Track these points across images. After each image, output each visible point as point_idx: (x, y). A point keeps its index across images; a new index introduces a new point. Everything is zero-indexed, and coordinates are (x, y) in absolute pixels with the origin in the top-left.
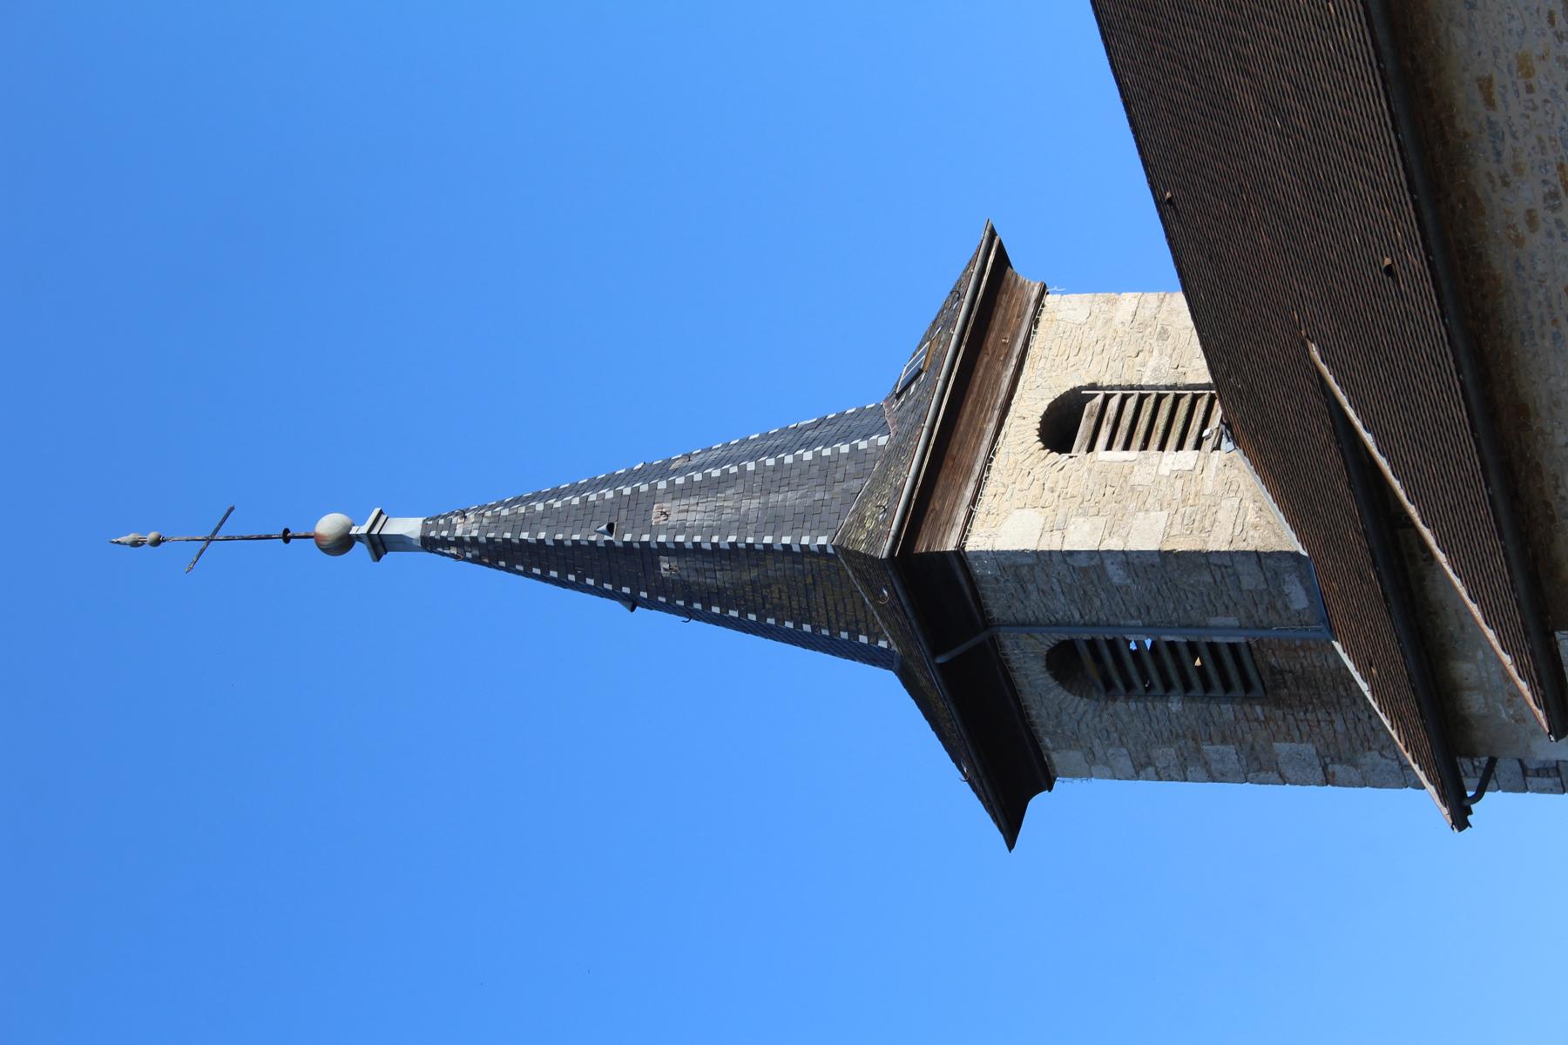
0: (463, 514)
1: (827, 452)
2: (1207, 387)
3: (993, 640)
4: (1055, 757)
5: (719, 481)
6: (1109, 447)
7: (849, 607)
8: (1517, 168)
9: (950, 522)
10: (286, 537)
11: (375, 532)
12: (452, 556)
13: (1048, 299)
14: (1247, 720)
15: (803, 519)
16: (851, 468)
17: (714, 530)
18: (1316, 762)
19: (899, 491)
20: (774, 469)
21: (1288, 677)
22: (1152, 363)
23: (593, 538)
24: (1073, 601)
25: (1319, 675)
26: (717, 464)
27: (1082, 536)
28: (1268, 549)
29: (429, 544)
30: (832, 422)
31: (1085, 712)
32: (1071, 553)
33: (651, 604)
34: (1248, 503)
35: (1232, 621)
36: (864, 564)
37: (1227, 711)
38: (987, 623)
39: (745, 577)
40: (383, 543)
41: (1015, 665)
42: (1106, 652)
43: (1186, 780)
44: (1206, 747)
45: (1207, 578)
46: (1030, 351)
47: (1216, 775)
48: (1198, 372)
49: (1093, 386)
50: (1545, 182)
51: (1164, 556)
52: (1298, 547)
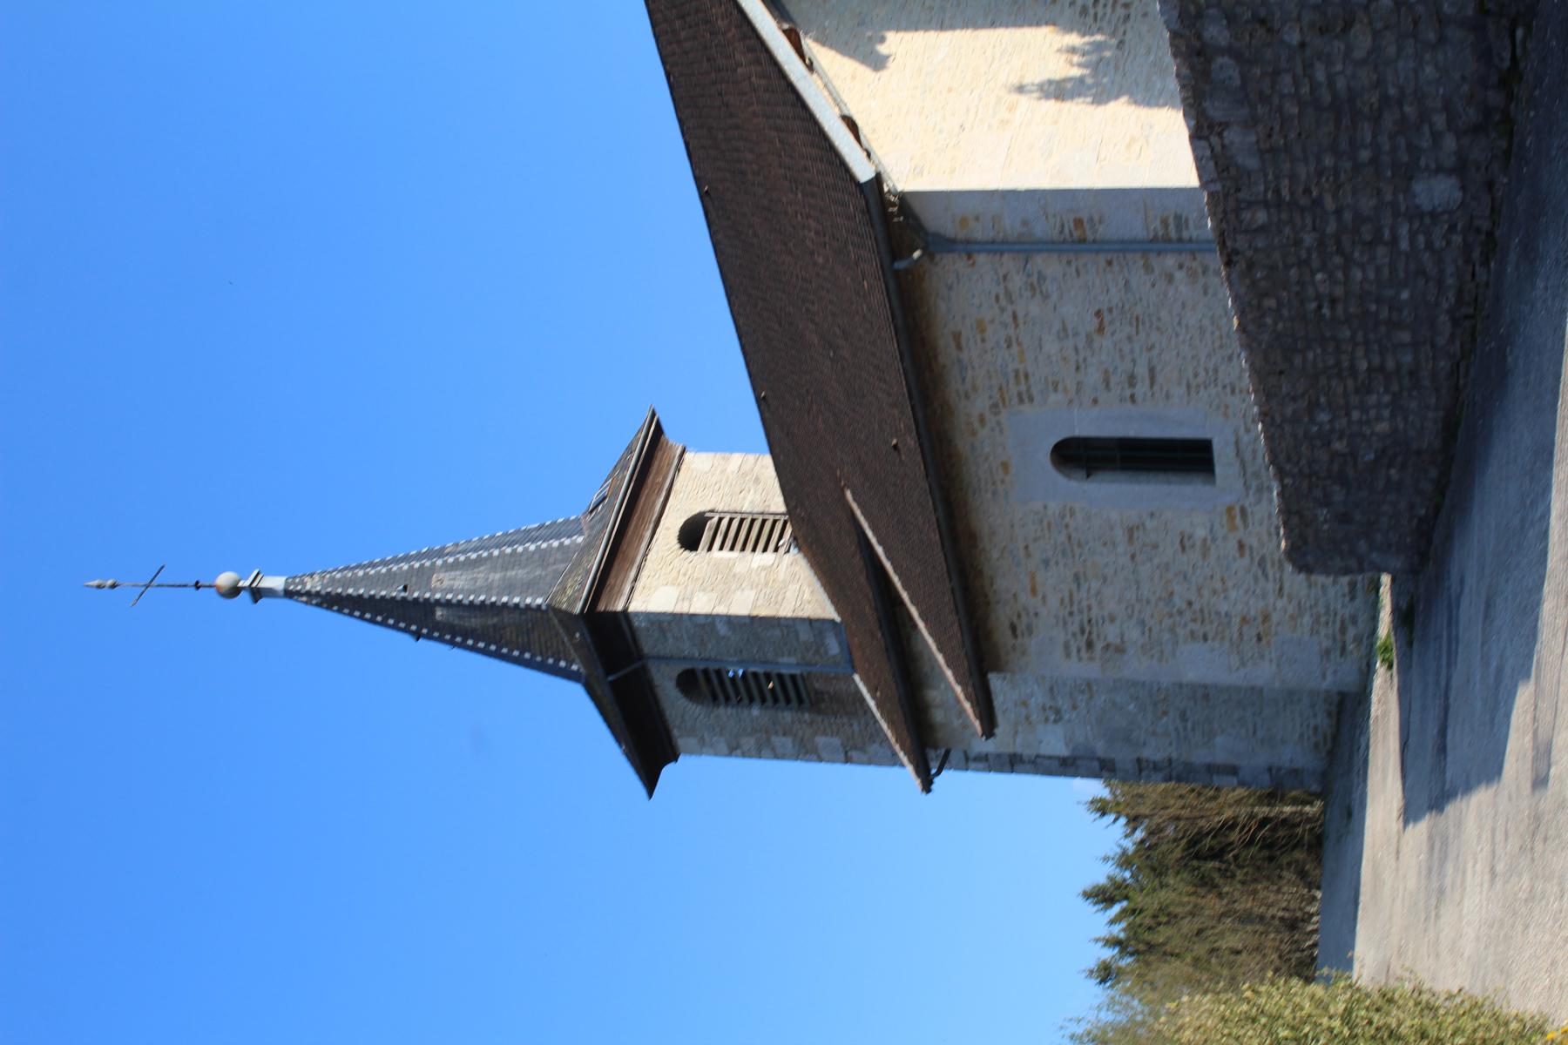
0: (311, 575)
1: (544, 546)
3: (644, 669)
6: (721, 548)
8: (975, 388)
9: (620, 592)
10: (197, 586)
11: (254, 585)
13: (687, 456)
15: (527, 587)
16: (559, 556)
17: (473, 592)
18: (841, 749)
19: (588, 572)
21: (826, 696)
22: (749, 498)
26: (475, 550)
27: (702, 604)
29: (289, 594)
31: (699, 715)
33: (429, 637)
35: (793, 660)
36: (565, 617)
37: (787, 716)
38: (641, 656)
39: (490, 622)
44: (774, 739)
46: (675, 488)
48: (777, 504)
49: (712, 511)
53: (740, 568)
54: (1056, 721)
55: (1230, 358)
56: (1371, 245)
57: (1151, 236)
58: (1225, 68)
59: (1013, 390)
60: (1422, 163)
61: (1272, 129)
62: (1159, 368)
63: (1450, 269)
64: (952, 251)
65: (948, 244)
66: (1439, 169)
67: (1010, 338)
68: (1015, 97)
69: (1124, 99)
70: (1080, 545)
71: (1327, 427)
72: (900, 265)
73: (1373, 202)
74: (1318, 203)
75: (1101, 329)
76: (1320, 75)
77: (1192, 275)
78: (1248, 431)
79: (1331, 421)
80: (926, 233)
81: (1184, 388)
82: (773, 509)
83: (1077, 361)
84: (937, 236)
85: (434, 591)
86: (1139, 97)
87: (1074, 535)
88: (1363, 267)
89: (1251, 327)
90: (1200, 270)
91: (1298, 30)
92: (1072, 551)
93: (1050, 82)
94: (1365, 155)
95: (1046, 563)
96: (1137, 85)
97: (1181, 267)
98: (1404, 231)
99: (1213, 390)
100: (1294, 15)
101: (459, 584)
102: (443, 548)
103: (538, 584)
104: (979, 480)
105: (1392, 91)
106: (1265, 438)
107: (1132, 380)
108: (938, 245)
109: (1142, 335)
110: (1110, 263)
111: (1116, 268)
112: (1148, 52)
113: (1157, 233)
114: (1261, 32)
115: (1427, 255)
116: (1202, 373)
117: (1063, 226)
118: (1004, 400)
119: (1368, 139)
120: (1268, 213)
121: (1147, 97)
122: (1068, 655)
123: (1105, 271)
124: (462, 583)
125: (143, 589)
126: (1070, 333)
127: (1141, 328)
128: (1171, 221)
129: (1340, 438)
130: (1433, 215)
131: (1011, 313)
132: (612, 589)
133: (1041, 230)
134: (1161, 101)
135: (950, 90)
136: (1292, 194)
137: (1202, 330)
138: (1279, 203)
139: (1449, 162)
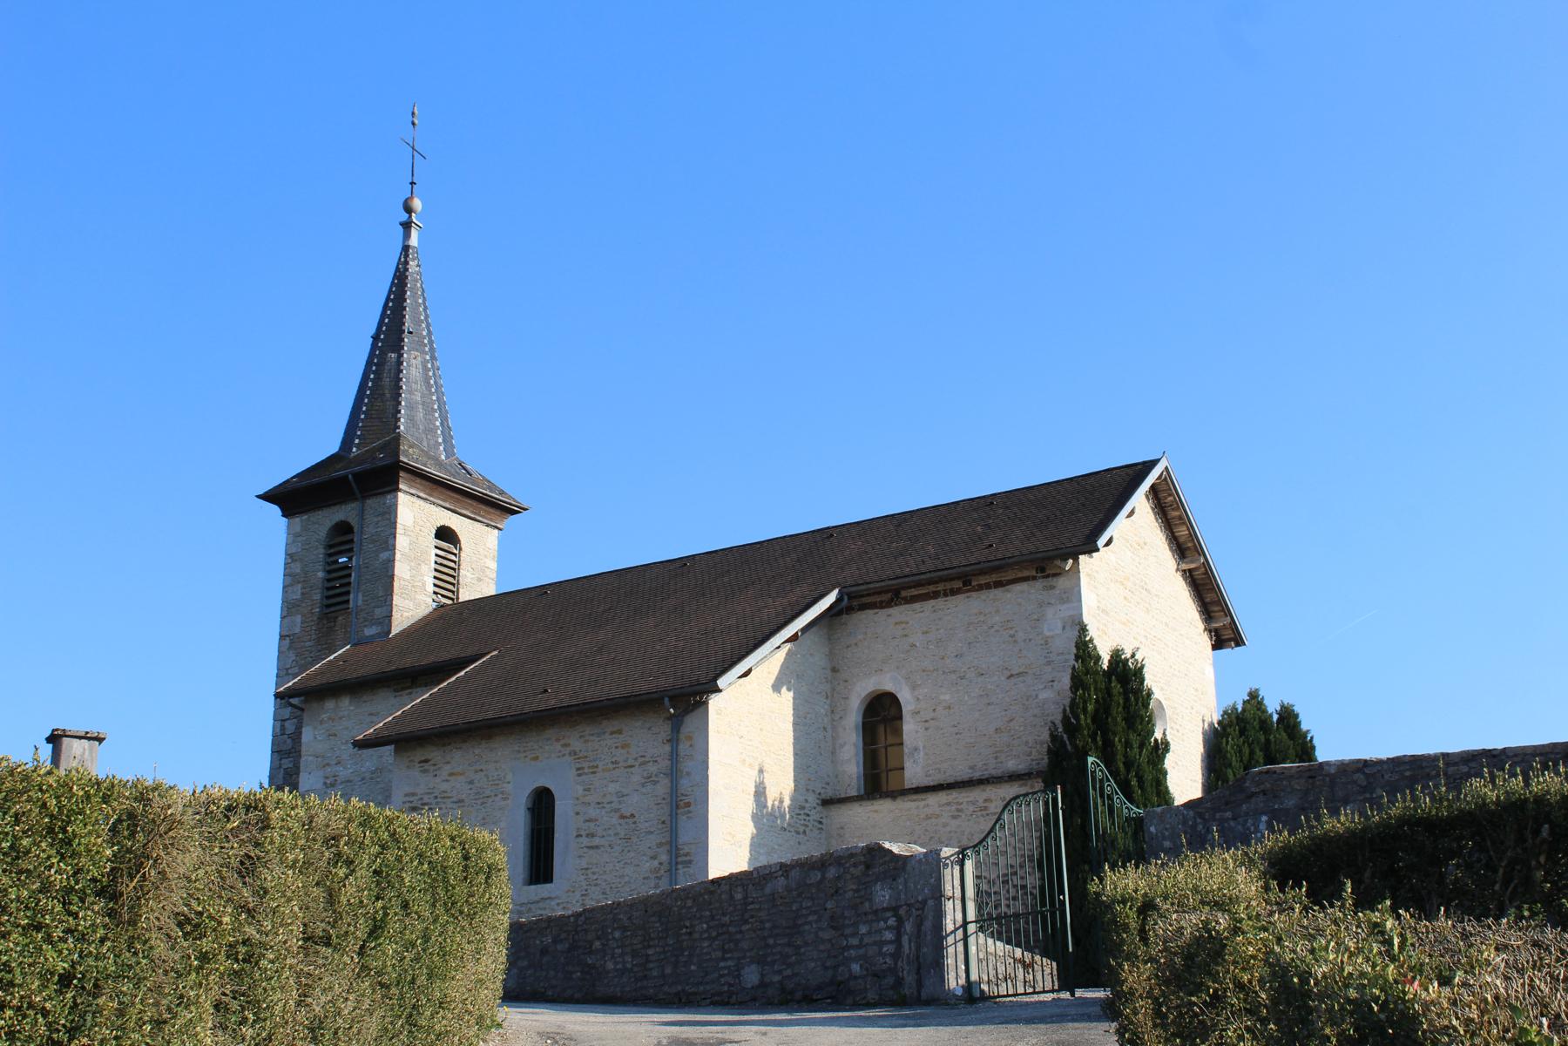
0: (418, 266)
1: (439, 432)
2: (458, 598)
3: (356, 499)
6: (437, 555)
7: (371, 437)
8: (586, 741)
9: (411, 487)
10: (412, 183)
12: (400, 259)
13: (496, 531)
15: (411, 419)
16: (432, 442)
19: (425, 465)
20: (432, 408)
21: (332, 624)
22: (468, 574)
25: (332, 637)
26: (435, 382)
27: (402, 542)
29: (406, 248)
30: (449, 434)
31: (318, 535)
32: (395, 537)
33: (374, 346)
34: (411, 613)
35: (360, 603)
37: (317, 597)
38: (364, 498)
39: (387, 391)
41: (343, 507)
42: (347, 547)
43: (284, 576)
44: (300, 586)
45: (381, 594)
46: (476, 523)
48: (465, 596)
49: (460, 549)
50: (580, 751)
54: (325, 783)
55: (604, 893)
59: (585, 765)
62: (599, 851)
63: (708, 987)
66: (762, 975)
68: (757, 768)
69: (755, 832)
70: (483, 803)
71: (610, 937)
72: (666, 700)
73: (746, 947)
74: (746, 922)
75: (623, 817)
76: (810, 918)
77: (657, 870)
78: (558, 904)
79: (614, 938)
80: (683, 716)
81: (585, 866)
84: (682, 721)
85: (409, 354)
86: (755, 840)
87: (490, 800)
88: (710, 945)
89: (675, 895)
90: (658, 875)
92: (479, 799)
93: (765, 788)
94: (771, 941)
95: (471, 782)
96: (762, 839)
97: (661, 864)
98: (730, 963)
99: (584, 883)
101: (413, 371)
102: (436, 360)
103: (413, 427)
104: (527, 743)
105: (803, 950)
106: (603, 906)
108: (676, 723)
109: (619, 842)
111: (660, 826)
113: (682, 849)
114: (833, 891)
115: (716, 975)
116: (595, 877)
117: (686, 795)
118: (578, 758)
119: (778, 942)
120: (740, 900)
121: (755, 845)
122: (406, 795)
124: (414, 373)
125: (411, 144)
127: (624, 841)
128: (688, 858)
129: (603, 945)
130: (739, 976)
133: (684, 783)
135: (761, 730)
136: (751, 909)
137: (622, 876)
138: (746, 904)
139: (767, 980)
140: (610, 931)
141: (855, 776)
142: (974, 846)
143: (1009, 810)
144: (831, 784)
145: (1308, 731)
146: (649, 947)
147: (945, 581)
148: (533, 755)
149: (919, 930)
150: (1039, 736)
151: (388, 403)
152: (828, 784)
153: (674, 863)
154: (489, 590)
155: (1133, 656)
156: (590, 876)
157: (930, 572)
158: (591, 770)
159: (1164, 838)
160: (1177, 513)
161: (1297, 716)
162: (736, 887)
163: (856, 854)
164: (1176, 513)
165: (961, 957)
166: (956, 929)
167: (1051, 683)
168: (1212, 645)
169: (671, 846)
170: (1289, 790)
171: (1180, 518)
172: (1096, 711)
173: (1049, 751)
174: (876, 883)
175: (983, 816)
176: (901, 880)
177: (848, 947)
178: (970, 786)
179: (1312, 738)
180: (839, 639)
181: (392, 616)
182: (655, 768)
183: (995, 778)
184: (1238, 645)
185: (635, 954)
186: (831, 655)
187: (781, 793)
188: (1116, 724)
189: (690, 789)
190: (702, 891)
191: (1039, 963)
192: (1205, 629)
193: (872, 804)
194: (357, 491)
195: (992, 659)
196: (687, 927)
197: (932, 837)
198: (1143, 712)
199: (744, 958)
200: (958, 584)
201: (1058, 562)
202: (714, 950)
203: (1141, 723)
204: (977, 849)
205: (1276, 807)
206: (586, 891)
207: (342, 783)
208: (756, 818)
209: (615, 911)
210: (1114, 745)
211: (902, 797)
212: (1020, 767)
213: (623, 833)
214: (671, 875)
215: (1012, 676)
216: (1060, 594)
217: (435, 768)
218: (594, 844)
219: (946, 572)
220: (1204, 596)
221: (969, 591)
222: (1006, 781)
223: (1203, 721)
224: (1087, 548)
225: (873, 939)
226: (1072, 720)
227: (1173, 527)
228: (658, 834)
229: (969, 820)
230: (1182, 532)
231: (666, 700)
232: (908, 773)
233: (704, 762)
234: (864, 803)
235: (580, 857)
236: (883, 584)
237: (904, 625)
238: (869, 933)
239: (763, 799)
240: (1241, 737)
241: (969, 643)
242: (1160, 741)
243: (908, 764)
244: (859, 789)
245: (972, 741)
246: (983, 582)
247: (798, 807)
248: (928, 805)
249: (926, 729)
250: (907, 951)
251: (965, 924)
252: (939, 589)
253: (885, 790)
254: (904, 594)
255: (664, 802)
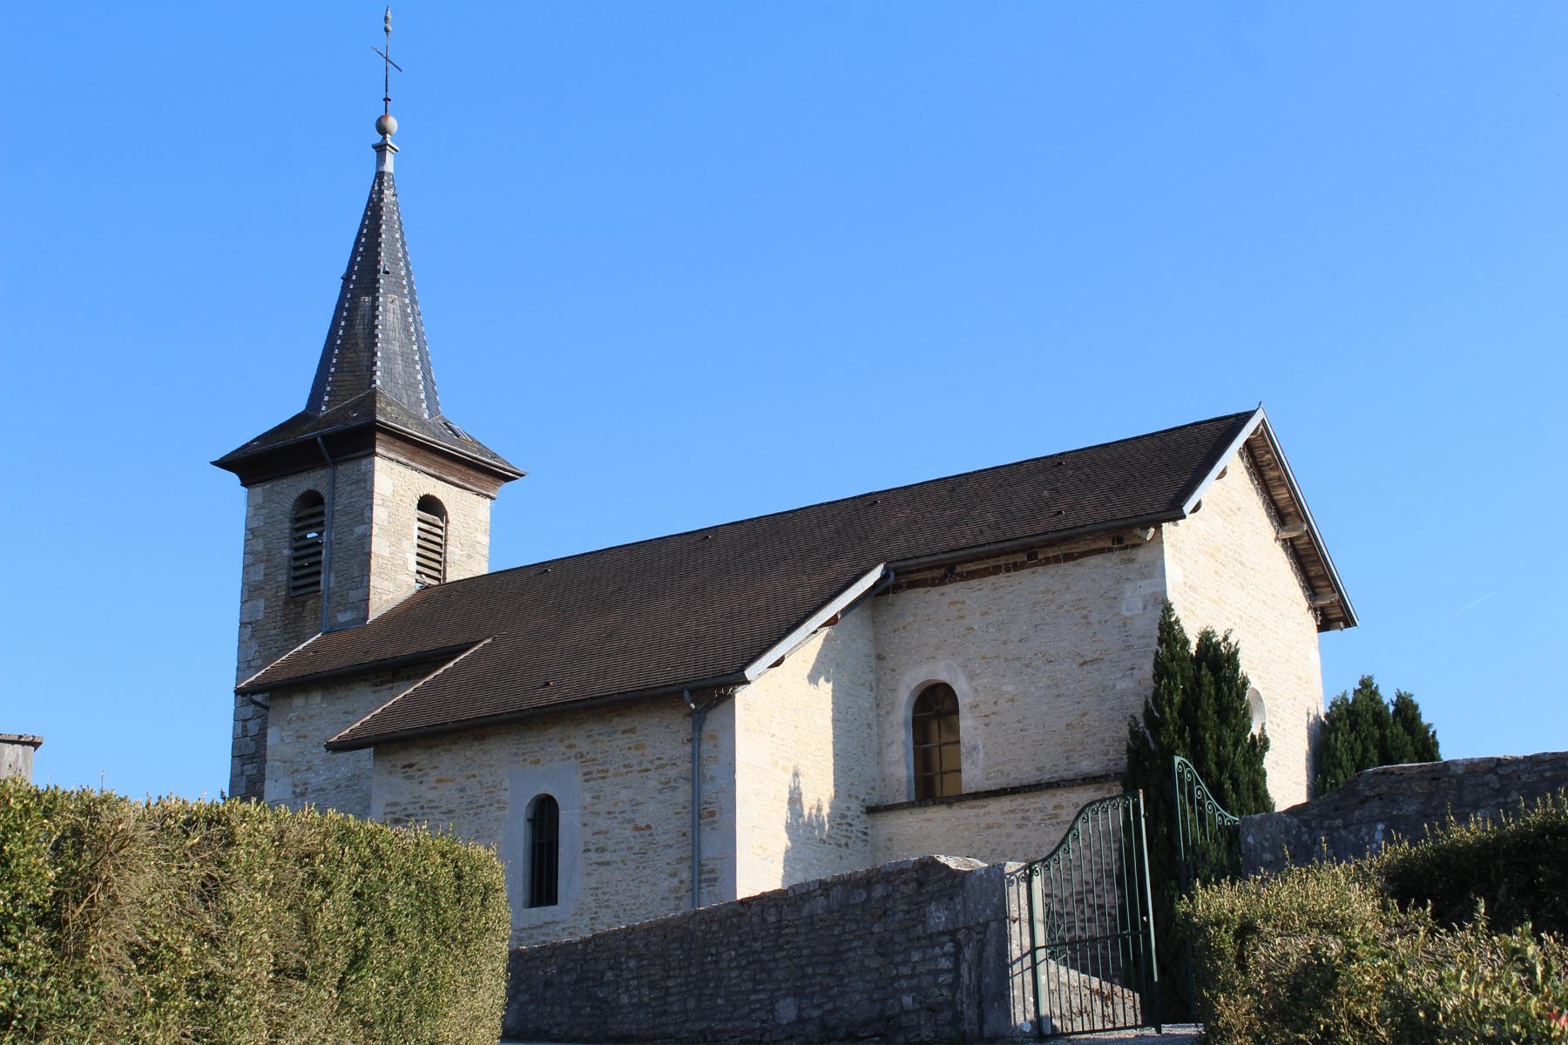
1: (421, 387)
2: (445, 578)
3: (325, 465)
4: (259, 489)
5: (408, 330)
6: (420, 529)
7: (343, 393)
8: (595, 742)
9: (389, 450)
10: (386, 100)
11: (388, 148)
12: (373, 187)
13: (488, 500)
14: (277, 587)
15: (389, 372)
16: (413, 399)
17: (384, 326)
18: (253, 619)
21: (301, 609)
23: (381, 263)
24: (346, 507)
26: (416, 329)
27: (379, 514)
28: (370, 605)
29: (380, 175)
31: (283, 506)
32: (372, 509)
33: (344, 288)
34: (391, 596)
35: (332, 585)
36: (372, 411)
37: (283, 577)
38: (335, 464)
39: (360, 341)
40: (382, 151)
41: (311, 474)
47: (247, 569)
48: (453, 575)
49: (447, 522)
50: (588, 753)
51: (369, 554)
52: (371, 619)
53: (405, 543)
54: (294, 792)
56: (754, 980)
57: (702, 862)
58: (860, 896)
59: (594, 769)
60: (804, 1001)
61: (825, 921)
62: (610, 868)
63: (737, 1024)
64: (693, 729)
65: (698, 726)
66: (800, 1010)
67: (631, 767)
68: (791, 771)
69: (789, 845)
70: (476, 814)
71: (624, 967)
72: (686, 694)
74: (781, 948)
75: (637, 828)
76: (855, 944)
77: (676, 890)
78: (563, 929)
79: (628, 968)
80: (706, 712)
82: (448, 570)
83: (614, 812)
84: (704, 719)
86: (790, 854)
87: (485, 810)
88: (740, 976)
89: (698, 917)
90: (679, 895)
91: (880, 930)
92: (472, 808)
93: (800, 794)
94: (810, 971)
95: (462, 790)
96: (798, 852)
97: (682, 882)
98: (762, 996)
99: (593, 905)
100: (887, 928)
101: (390, 317)
105: (846, 980)
107: (601, 850)
108: (698, 719)
109: (633, 857)
110: (684, 834)
111: (681, 839)
112: (818, 860)
113: (707, 865)
114: (880, 912)
115: (747, 1010)
116: (606, 898)
118: (586, 762)
119: (818, 971)
121: (790, 860)
123: (679, 831)
126: (635, 808)
128: (713, 875)
129: (616, 975)
130: (773, 1011)
131: (649, 767)
132: (392, 444)
133: (708, 789)
134: (787, 868)
135: (795, 727)
136: (787, 934)
138: (780, 928)
139: (805, 1015)
140: (623, 959)
141: (904, 779)
142: (1044, 860)
143: (1084, 818)
144: (876, 789)
145: (1430, 725)
146: (669, 977)
147: (1007, 553)
148: (534, 759)
149: (980, 959)
150: (1117, 732)
151: (362, 354)
152: (874, 789)
153: (696, 882)
154: (481, 568)
155: (1226, 639)
156: (601, 896)
157: (989, 544)
158: (601, 775)
159: (1264, 850)
160: (1275, 474)
161: (1416, 707)
162: (769, 908)
163: (907, 869)
164: (1275, 474)
165: (1029, 988)
166: (1024, 956)
167: (1129, 672)
168: (1318, 626)
169: (693, 861)
170: (1409, 793)
171: (1280, 478)
172: (1184, 703)
173: (1129, 750)
174: (930, 903)
175: (1053, 825)
176: (958, 900)
177: (898, 977)
178: (1037, 791)
179: (1434, 733)
180: (885, 622)
181: (369, 599)
182: (674, 772)
183: (1066, 781)
184: (1347, 625)
185: (652, 986)
186: (876, 640)
187: (819, 800)
188: (1207, 718)
189: (714, 796)
190: (730, 914)
191: (1120, 994)
192: (1310, 608)
193: (925, 812)
194: (327, 457)
195: (1063, 644)
196: (712, 955)
197: (994, 850)
198: (1237, 704)
199: (779, 989)
200: (1022, 557)
201: (1138, 532)
202: (744, 981)
203: (1235, 717)
204: (1046, 863)
205: (1394, 813)
206: (596, 913)
207: (314, 791)
208: (790, 828)
209: (630, 937)
210: (1204, 743)
211: (958, 804)
212: (1095, 768)
213: (638, 848)
214: (693, 894)
215: (1085, 662)
216: (1140, 567)
217: (421, 773)
218: (605, 860)
219: (1007, 544)
220: (1309, 569)
221: (1035, 565)
222: (1080, 785)
223: (1308, 714)
224: (1169, 515)
225: (926, 967)
226: (1156, 714)
227: (1271, 489)
228: (677, 848)
229: (1036, 830)
230: (1282, 495)
231: (686, 694)
232: (965, 776)
233: (730, 764)
234: (915, 811)
235: (589, 874)
236: (935, 558)
237: (959, 606)
238: (923, 960)
239: (798, 807)
240: (1352, 732)
241: (1036, 626)
242: (1257, 738)
243: (966, 766)
244: (909, 795)
245: (1040, 738)
246: (1050, 555)
247: (840, 816)
248: (989, 813)
249: (987, 725)
250: (966, 981)
251: (1033, 950)
252: (1000, 563)
253: (939, 795)
254: (959, 569)
255: (684, 810)
